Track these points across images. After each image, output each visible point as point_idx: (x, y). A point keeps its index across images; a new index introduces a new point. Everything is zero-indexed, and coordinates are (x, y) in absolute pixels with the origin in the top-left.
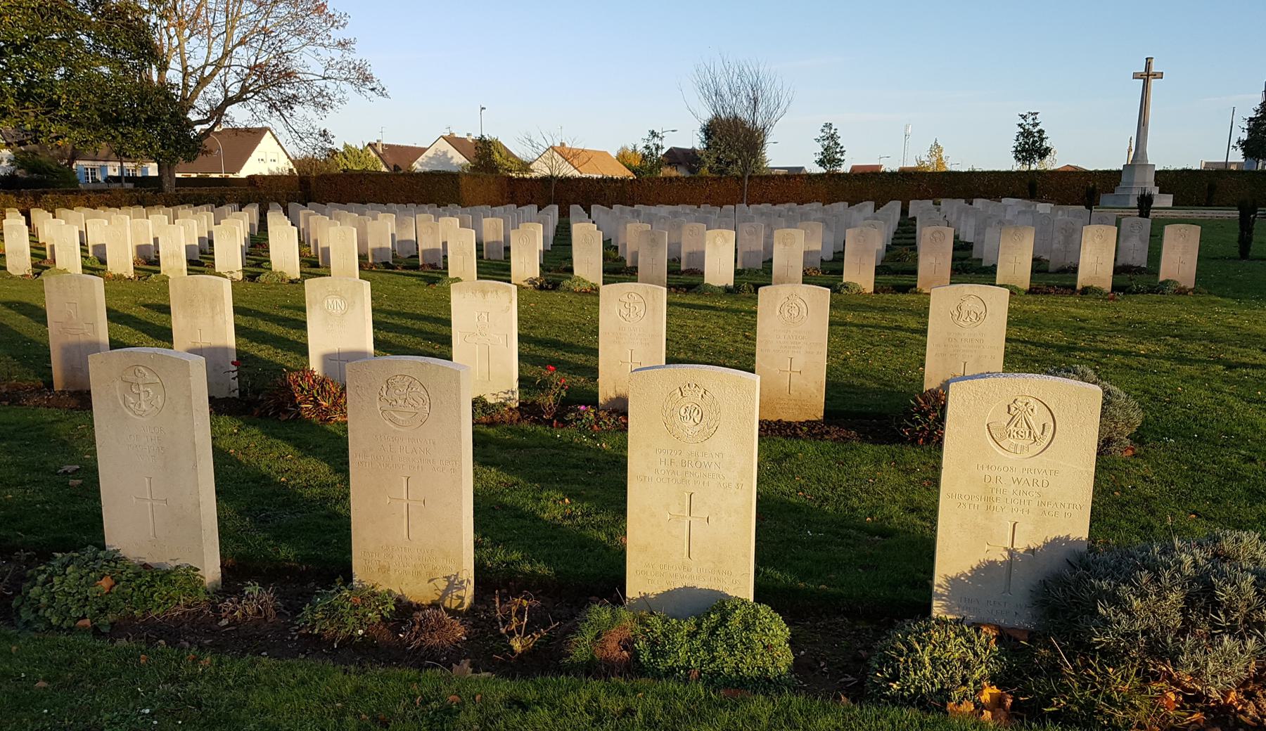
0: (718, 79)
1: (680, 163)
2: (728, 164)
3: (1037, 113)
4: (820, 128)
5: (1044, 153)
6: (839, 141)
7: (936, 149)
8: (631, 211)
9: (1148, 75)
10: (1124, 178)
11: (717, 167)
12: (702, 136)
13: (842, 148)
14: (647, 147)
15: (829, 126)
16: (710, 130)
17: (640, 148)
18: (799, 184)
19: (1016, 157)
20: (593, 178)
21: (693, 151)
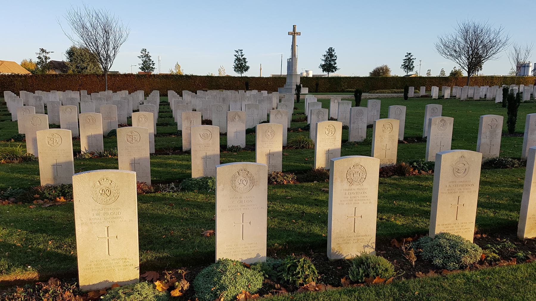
0: (83, 19)
1: (57, 68)
2: (82, 69)
3: (242, 50)
4: (296, 26)
5: (247, 69)
6: (151, 58)
7: (178, 66)
8: (34, 97)
9: (295, 34)
10: (288, 81)
11: (77, 70)
12: (67, 55)
13: (153, 62)
14: (39, 58)
15: (145, 50)
16: (71, 53)
17: (36, 60)
18: (133, 79)
19: (235, 70)
20: (5, 75)
21: (63, 63)
